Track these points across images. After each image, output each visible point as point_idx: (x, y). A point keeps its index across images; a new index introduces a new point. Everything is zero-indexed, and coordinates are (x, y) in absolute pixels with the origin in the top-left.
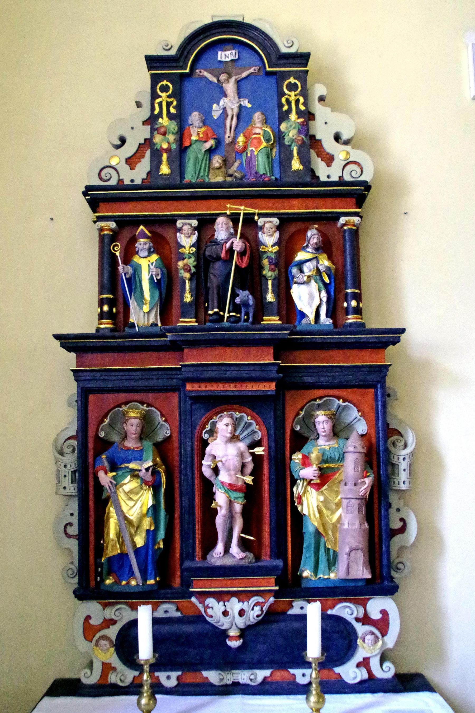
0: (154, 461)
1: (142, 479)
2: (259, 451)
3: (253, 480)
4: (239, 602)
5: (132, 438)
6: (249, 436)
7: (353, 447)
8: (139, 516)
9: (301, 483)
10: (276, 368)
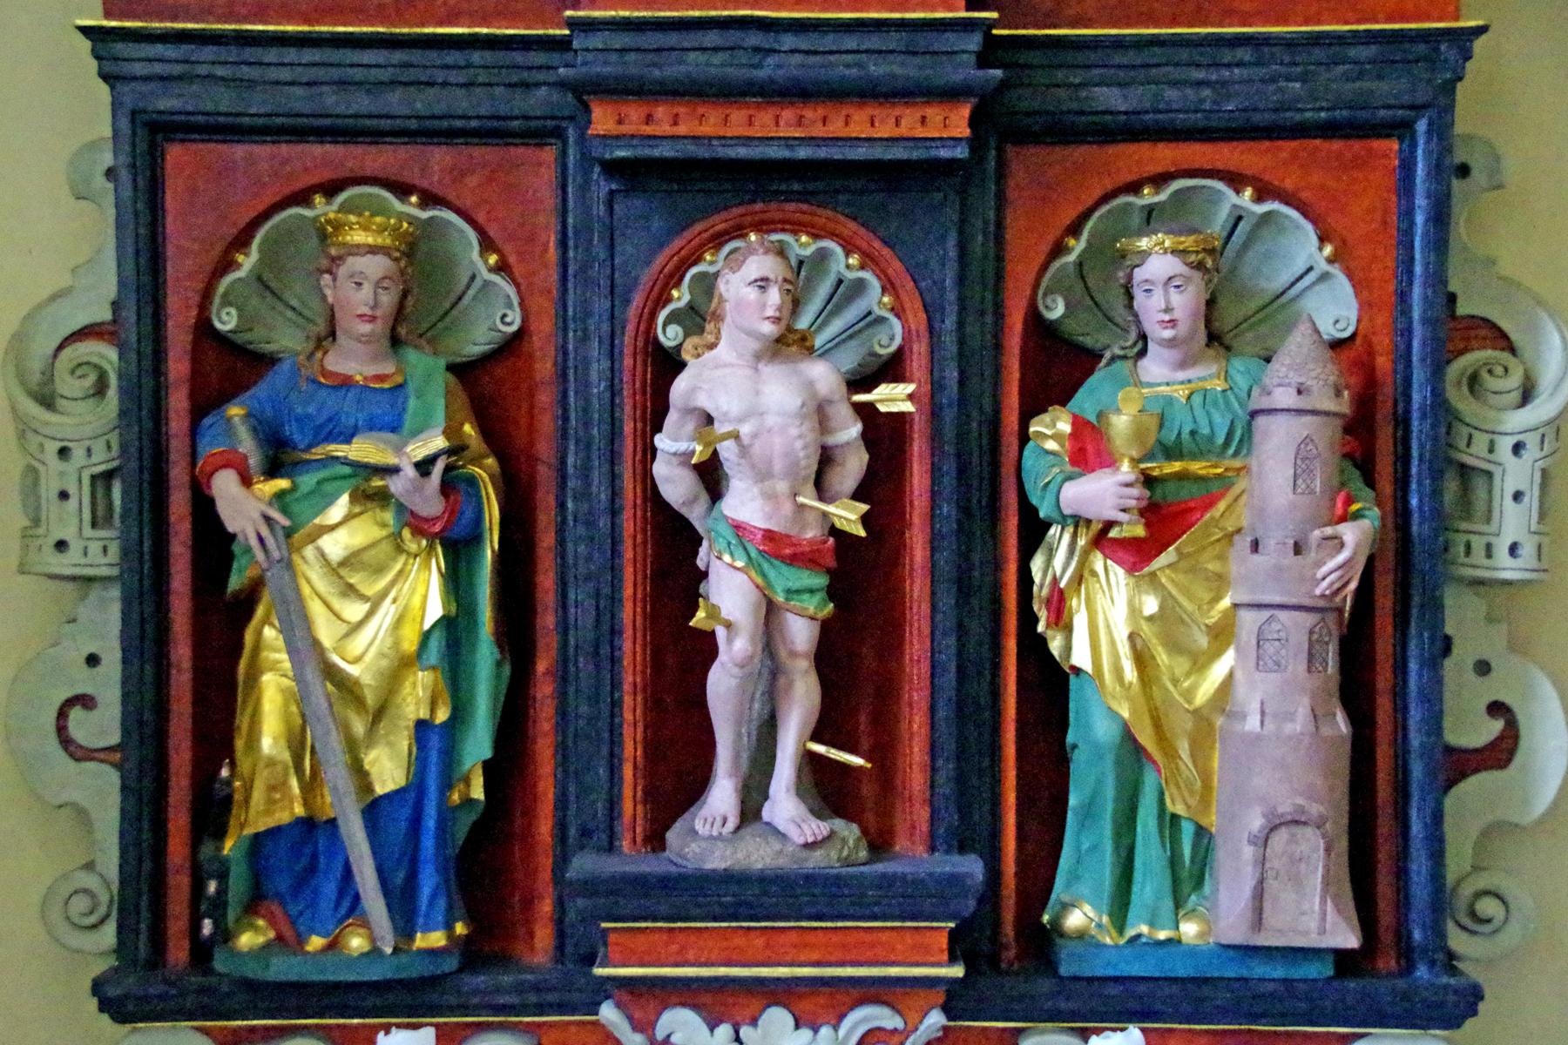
0: (451, 431)
1: (401, 508)
2: (892, 397)
3: (865, 520)
4: (797, 1026)
5: (359, 339)
6: (851, 337)
7: (1294, 397)
8: (384, 663)
9: (1067, 538)
10: (974, 42)
